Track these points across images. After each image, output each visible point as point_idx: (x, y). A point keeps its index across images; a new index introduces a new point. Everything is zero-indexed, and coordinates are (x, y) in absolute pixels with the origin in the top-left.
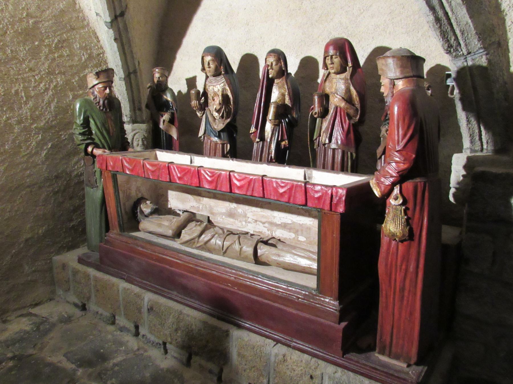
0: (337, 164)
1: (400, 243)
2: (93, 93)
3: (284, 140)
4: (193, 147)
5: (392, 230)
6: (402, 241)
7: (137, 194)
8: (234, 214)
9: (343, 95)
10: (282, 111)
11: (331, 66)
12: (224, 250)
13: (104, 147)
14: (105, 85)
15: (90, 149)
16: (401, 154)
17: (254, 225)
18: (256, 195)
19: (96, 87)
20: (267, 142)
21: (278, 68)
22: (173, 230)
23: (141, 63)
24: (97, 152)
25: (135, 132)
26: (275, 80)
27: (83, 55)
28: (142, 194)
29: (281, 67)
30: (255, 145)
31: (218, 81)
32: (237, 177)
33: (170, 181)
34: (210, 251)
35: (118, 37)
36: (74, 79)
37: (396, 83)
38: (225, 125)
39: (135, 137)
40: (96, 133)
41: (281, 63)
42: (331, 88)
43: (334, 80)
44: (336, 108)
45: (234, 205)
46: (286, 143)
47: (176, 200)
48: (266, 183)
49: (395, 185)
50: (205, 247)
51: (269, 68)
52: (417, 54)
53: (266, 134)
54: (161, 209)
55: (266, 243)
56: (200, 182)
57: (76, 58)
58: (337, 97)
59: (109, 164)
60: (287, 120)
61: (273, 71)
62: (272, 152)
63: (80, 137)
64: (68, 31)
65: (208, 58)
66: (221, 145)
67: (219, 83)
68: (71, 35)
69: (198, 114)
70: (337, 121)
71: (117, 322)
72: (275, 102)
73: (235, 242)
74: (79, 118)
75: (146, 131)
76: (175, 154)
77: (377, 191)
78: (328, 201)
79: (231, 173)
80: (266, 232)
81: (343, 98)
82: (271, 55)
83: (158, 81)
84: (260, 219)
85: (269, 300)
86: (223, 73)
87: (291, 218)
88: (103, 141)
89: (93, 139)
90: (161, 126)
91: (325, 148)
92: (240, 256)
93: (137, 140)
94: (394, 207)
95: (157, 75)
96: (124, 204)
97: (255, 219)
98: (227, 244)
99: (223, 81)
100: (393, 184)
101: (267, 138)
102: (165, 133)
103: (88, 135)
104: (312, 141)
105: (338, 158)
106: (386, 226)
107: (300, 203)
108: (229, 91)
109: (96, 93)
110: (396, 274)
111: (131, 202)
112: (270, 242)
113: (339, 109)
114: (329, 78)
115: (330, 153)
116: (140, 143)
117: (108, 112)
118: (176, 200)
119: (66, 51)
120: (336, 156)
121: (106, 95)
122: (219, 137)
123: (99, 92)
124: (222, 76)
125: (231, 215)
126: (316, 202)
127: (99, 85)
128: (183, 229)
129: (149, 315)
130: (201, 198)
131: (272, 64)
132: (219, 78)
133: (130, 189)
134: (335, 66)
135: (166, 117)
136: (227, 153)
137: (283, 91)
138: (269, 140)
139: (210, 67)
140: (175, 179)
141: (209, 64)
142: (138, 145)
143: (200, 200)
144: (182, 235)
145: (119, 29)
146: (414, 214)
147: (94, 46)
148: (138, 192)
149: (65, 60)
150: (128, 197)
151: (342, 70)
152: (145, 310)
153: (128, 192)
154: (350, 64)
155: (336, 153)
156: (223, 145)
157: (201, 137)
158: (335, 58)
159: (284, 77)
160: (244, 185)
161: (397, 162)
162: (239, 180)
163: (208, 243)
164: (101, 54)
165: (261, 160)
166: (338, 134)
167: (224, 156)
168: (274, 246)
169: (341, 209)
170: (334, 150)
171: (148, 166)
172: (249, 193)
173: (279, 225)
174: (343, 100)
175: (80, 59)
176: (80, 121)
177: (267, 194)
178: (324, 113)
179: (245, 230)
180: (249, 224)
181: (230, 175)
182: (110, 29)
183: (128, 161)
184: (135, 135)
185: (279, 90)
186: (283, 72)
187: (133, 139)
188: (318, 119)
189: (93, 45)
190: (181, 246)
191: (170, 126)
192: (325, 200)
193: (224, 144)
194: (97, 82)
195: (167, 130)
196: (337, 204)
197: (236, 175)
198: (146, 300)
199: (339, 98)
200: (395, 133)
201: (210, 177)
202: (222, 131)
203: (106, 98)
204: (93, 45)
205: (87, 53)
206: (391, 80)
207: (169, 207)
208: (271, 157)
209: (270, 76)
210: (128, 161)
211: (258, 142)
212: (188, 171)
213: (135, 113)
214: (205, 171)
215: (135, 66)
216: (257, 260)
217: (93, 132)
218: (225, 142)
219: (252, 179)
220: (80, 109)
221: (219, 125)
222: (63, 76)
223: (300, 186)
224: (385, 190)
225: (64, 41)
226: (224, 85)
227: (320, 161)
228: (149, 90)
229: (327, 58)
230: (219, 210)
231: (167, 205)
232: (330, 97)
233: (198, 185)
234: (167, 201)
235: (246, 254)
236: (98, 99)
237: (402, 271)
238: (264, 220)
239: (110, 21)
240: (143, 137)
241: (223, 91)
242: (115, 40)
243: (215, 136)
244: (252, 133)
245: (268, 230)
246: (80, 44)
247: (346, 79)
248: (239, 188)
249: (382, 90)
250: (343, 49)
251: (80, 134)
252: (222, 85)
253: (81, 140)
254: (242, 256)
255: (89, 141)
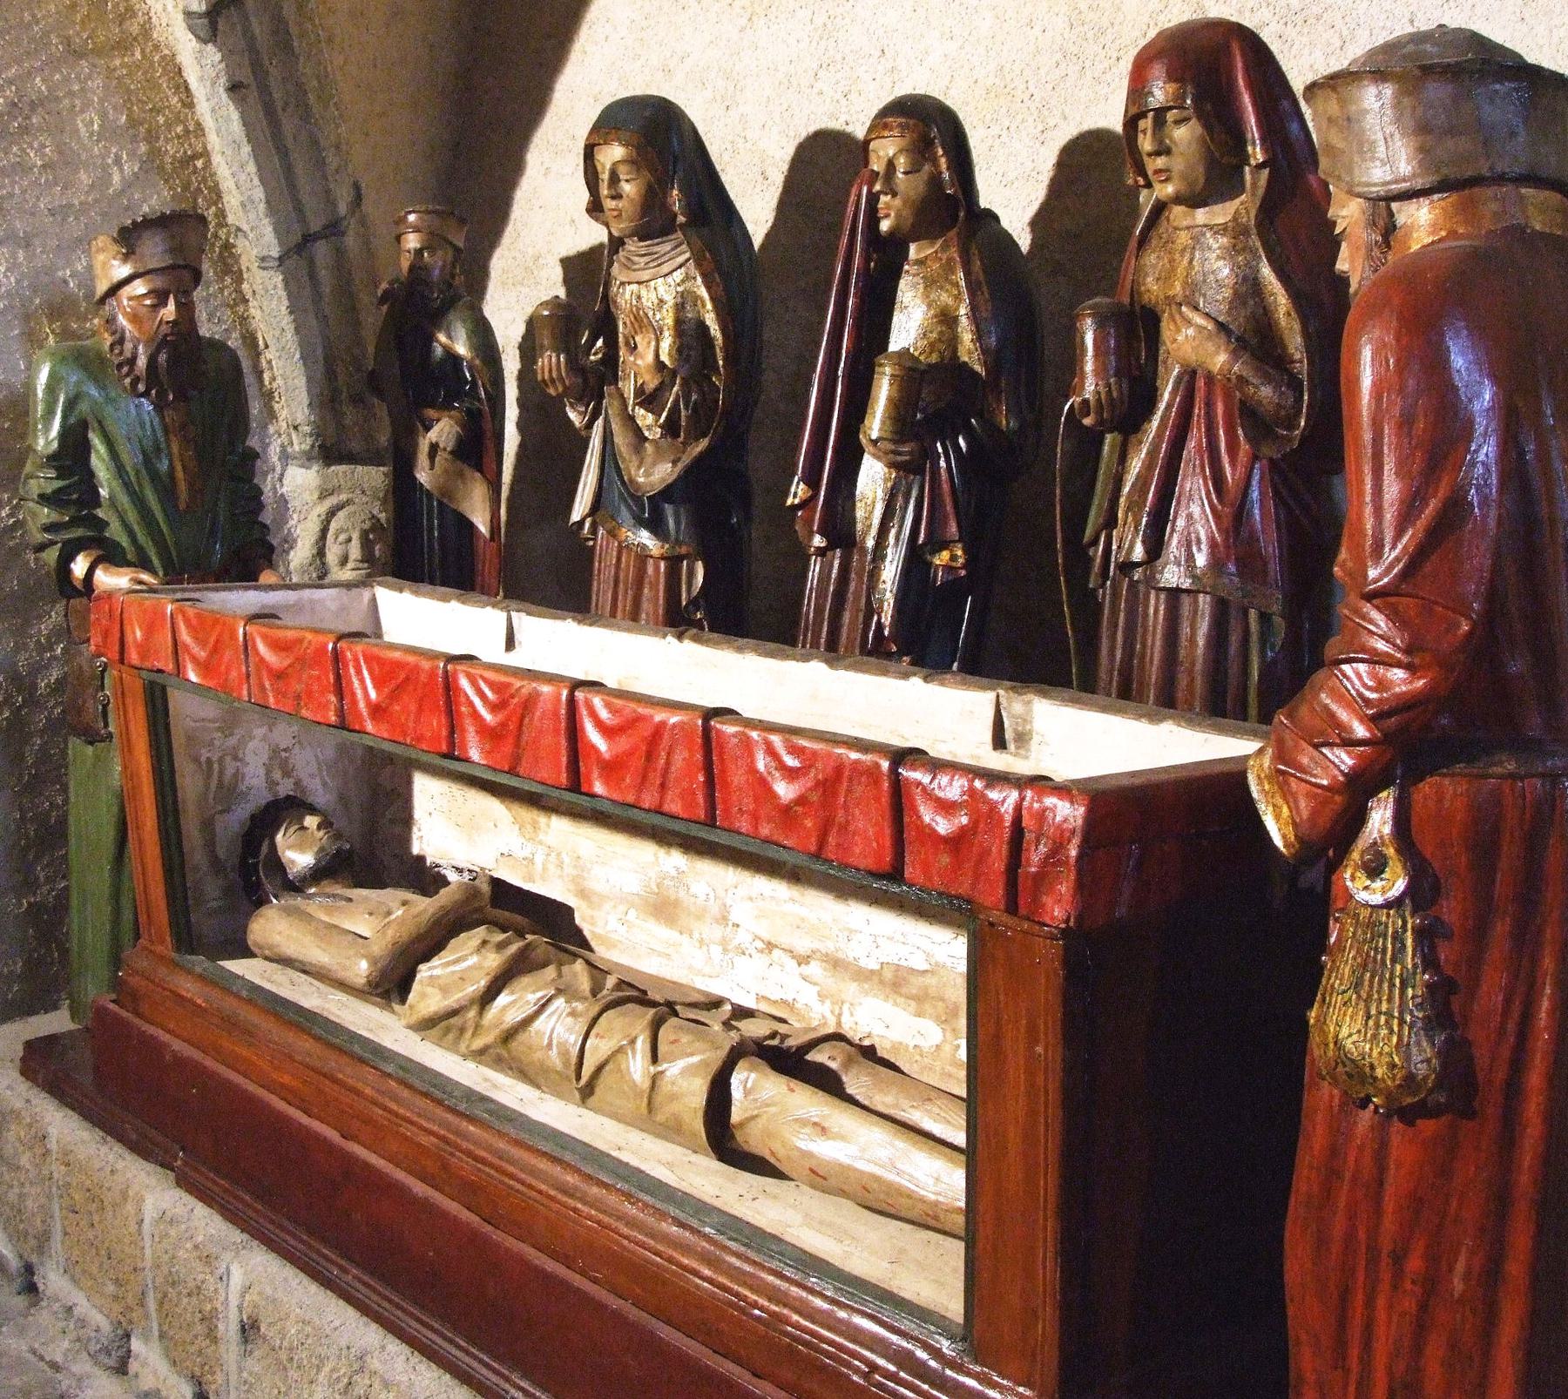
0: (1191, 672)
1: (1397, 1125)
2: (110, 321)
3: (945, 545)
4: (553, 575)
5: (1349, 1044)
6: (1408, 1115)
7: (272, 784)
8: (676, 904)
9: (1221, 311)
10: (937, 397)
11: (1160, 162)
12: (583, 1081)
13: (144, 564)
14: (159, 282)
15: (79, 567)
16: (1393, 615)
17: (760, 961)
18: (674, 806)
19: (127, 291)
20: (863, 550)
21: (921, 188)
22: (373, 961)
23: (369, 196)
24: (110, 580)
25: (332, 501)
26: (913, 248)
27: (118, 161)
28: (297, 783)
29: (935, 181)
30: (815, 567)
31: (658, 261)
32: (604, 714)
33: (342, 725)
34: (524, 1073)
35: (245, 75)
36: (69, 263)
37: (1401, 219)
38: (680, 466)
39: (333, 526)
40: (112, 498)
41: (934, 161)
42: (1166, 278)
43: (1183, 238)
44: (1190, 376)
45: (675, 860)
46: (953, 558)
47: (454, 827)
48: (721, 747)
49: (1373, 792)
50: (506, 1051)
51: (877, 187)
52: (1531, 58)
53: (860, 514)
54: (374, 851)
55: (790, 1060)
56: (452, 732)
57: (83, 175)
58: (1189, 323)
59: (129, 639)
60: (961, 442)
61: (897, 202)
62: (881, 601)
63: (46, 514)
64: (53, 64)
65: (613, 154)
66: (662, 565)
67: (666, 268)
68: (67, 79)
69: (572, 415)
70: (1191, 444)
71: (133, 1366)
72: (904, 353)
73: (633, 1042)
74: (47, 429)
75: (384, 502)
76: (445, 599)
77: (1277, 817)
78: (998, 861)
79: (579, 695)
80: (808, 1004)
81: (1221, 326)
82: (886, 126)
83: (412, 268)
84: (784, 940)
85: (738, 1361)
86: (681, 219)
87: (925, 944)
88: (142, 538)
89: (102, 525)
90: (423, 476)
91: (1133, 585)
92: (649, 1112)
93: (342, 537)
94: (1364, 914)
95: (412, 241)
96: (208, 825)
97: (767, 936)
98: (598, 1049)
99: (681, 259)
100: (1356, 793)
101: (865, 533)
102: (440, 503)
103: (80, 503)
104: (1078, 554)
105: (1192, 640)
106: (1323, 1021)
107: (868, 863)
108: (709, 306)
109: (122, 321)
110: (1370, 1302)
111: (242, 813)
112: (818, 1056)
113: (1201, 383)
114: (1163, 227)
115: (1156, 608)
116: (355, 551)
117: (168, 405)
118: (454, 827)
119: (43, 146)
120: (1185, 630)
121: (165, 329)
122: (655, 525)
123: (134, 318)
124: (679, 234)
125: (664, 908)
126: (945, 859)
127: (137, 282)
128: (426, 958)
129: (246, 1354)
130: (542, 819)
131: (891, 165)
132: (667, 247)
133: (236, 758)
134: (1177, 164)
135: (443, 431)
136: (693, 602)
137: (945, 298)
138: (870, 543)
139: (617, 196)
140: (358, 715)
141: (614, 179)
142: (344, 561)
143: (535, 826)
144: (416, 986)
145: (252, 48)
146: (1475, 962)
147: (169, 126)
148: (277, 775)
149: (36, 183)
150: (229, 792)
151: (1218, 179)
152: (229, 1328)
153: (230, 771)
154: (1257, 154)
155: (1186, 609)
156: (673, 562)
157: (581, 523)
158: (1178, 122)
159: (953, 233)
160: (630, 754)
161: (1376, 659)
162: (606, 730)
163: (522, 1037)
164: (195, 157)
165: (832, 646)
166: (1195, 516)
167: (677, 620)
168: (827, 1082)
169: (1058, 907)
170: (1175, 593)
171: (262, 648)
172: (648, 800)
173: (872, 972)
174: (1223, 338)
175: (105, 180)
176: (47, 438)
177: (726, 811)
178: (1131, 407)
179: (717, 988)
180: (741, 961)
181: (572, 701)
182: (205, 42)
183: (194, 622)
184: (332, 513)
185: (926, 295)
186: (953, 207)
187: (324, 531)
188: (1109, 438)
189: (161, 120)
190: (415, 1037)
191: (461, 475)
192: (985, 853)
193: (680, 558)
194: (124, 271)
195: (447, 492)
196: (1042, 880)
197: (597, 702)
198: (237, 1278)
199: (1200, 328)
200: (1361, 494)
201: (494, 708)
202: (668, 493)
203: (164, 343)
204: (161, 120)
205: (132, 154)
206: (1374, 200)
207: (415, 850)
208: (880, 626)
209: (885, 226)
210: (194, 622)
211: (821, 552)
212: (407, 679)
213: (338, 415)
214: (473, 681)
215: (331, 202)
216: (721, 1135)
217: (103, 492)
218: (684, 550)
219: (663, 724)
220: (51, 389)
221: (655, 473)
222: (21, 254)
223: (872, 772)
224: (1315, 813)
225: (33, 106)
226: (688, 278)
227: (1110, 652)
228: (385, 308)
229: (1142, 124)
230: (604, 875)
231: (406, 840)
232: (1164, 324)
233: (444, 748)
234: (407, 820)
235: (675, 1107)
236: (128, 346)
237: (1408, 1286)
238: (803, 945)
239: (204, 8)
240: (367, 525)
241: (680, 308)
242: (234, 88)
243: (640, 522)
244: (795, 508)
245: (822, 997)
246: (103, 116)
247: (1236, 230)
248: (611, 769)
249: (1342, 265)
250: (1214, 70)
251: (44, 499)
252: (678, 275)
253: (48, 528)
254: (660, 1118)
255: (79, 532)
